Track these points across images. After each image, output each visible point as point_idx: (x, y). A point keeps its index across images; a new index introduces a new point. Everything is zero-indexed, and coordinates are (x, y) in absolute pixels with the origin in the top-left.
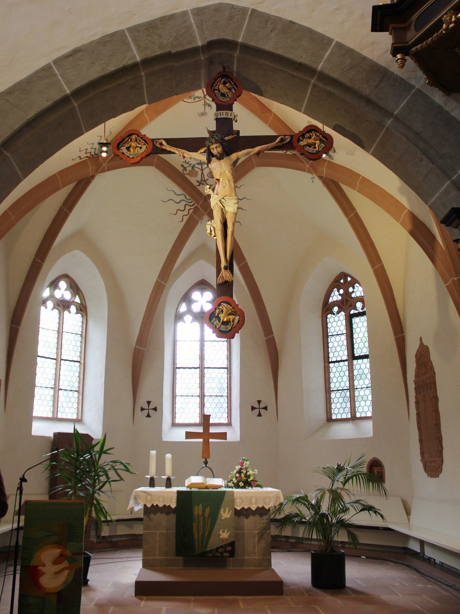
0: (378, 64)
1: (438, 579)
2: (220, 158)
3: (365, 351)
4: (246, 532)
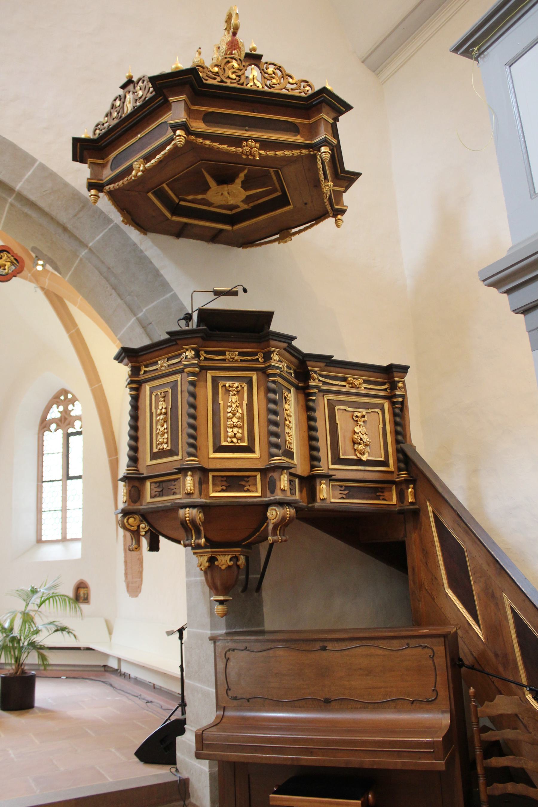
0: (80, 193)
1: (129, 691)
3: (80, 473)
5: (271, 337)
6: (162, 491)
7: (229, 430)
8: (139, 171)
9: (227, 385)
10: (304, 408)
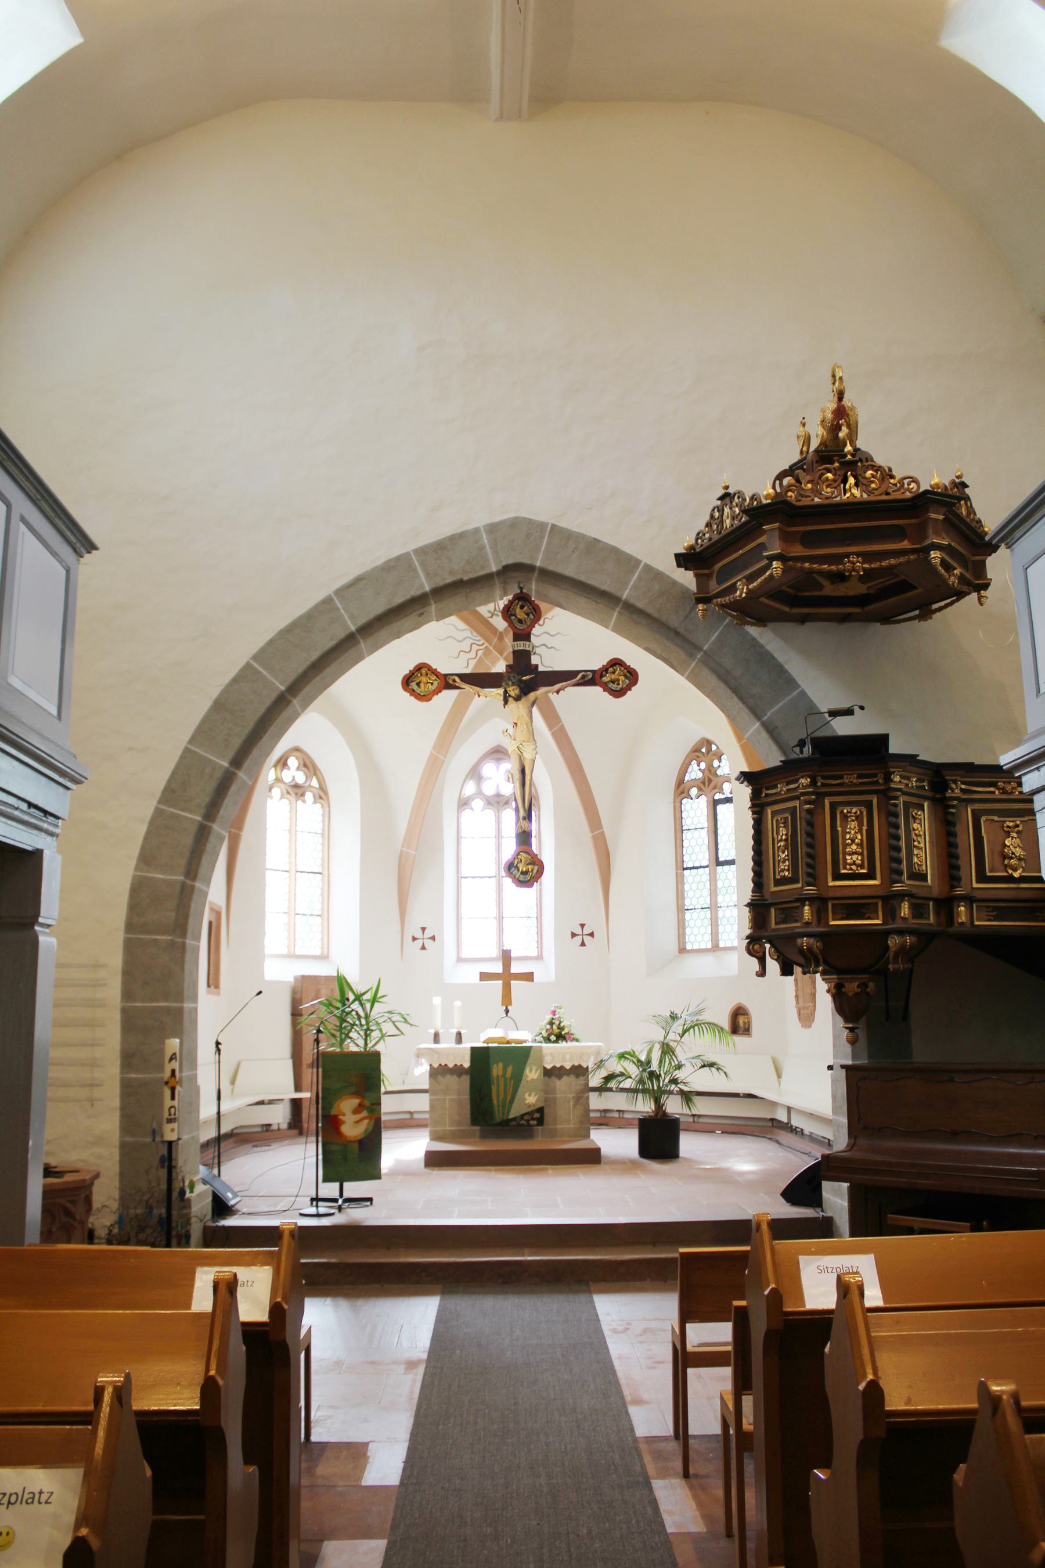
2: (517, 699)
4: (558, 1095)
7: (848, 857)
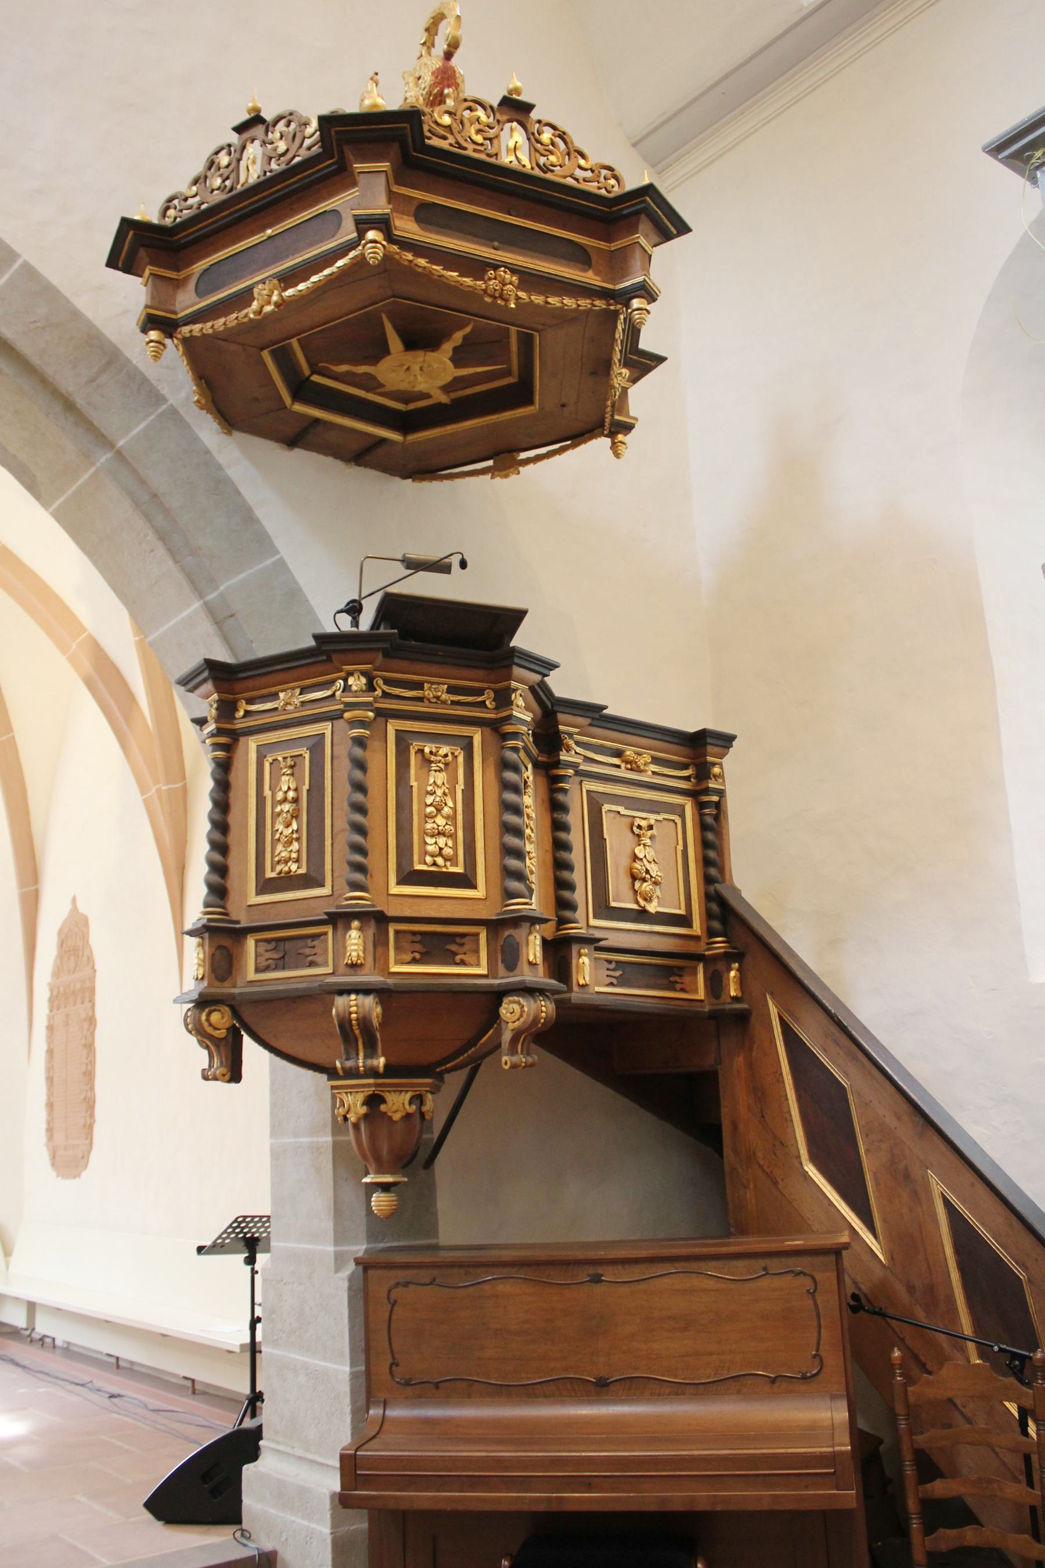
1: (59, 1375)
5: (516, 660)
6: (283, 957)
7: (429, 840)
8: (269, 303)
9: (427, 750)
10: (547, 804)
